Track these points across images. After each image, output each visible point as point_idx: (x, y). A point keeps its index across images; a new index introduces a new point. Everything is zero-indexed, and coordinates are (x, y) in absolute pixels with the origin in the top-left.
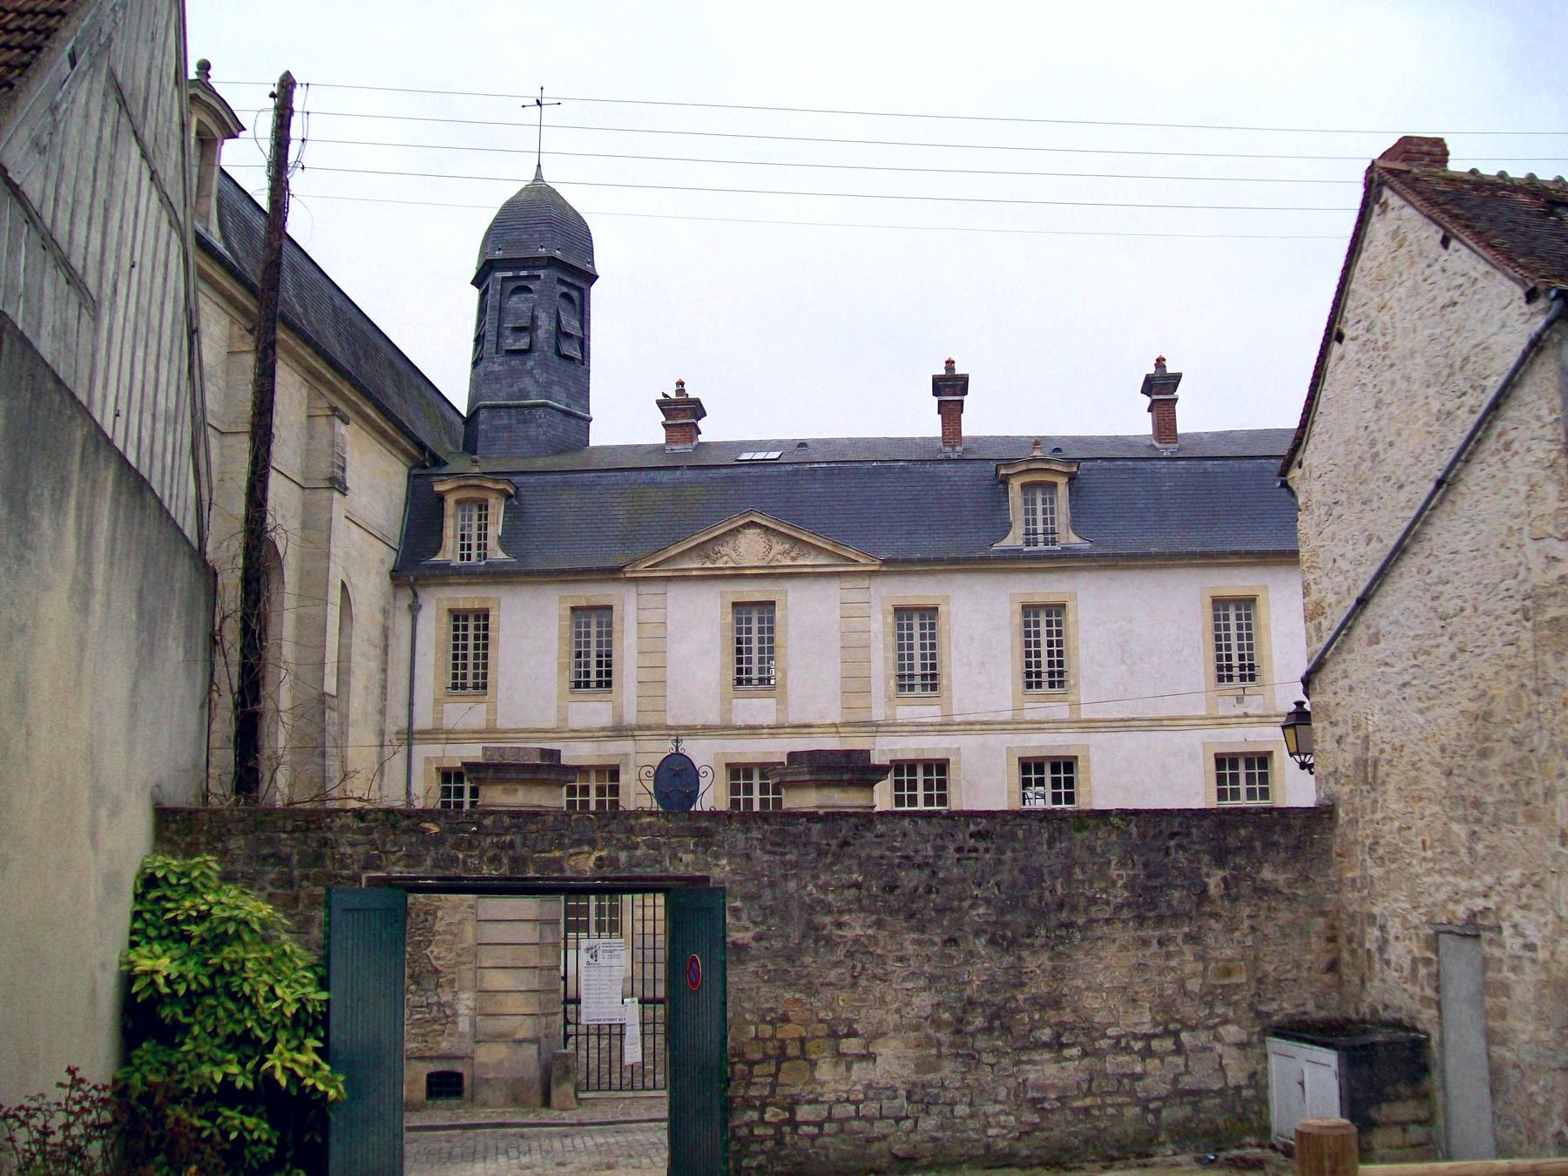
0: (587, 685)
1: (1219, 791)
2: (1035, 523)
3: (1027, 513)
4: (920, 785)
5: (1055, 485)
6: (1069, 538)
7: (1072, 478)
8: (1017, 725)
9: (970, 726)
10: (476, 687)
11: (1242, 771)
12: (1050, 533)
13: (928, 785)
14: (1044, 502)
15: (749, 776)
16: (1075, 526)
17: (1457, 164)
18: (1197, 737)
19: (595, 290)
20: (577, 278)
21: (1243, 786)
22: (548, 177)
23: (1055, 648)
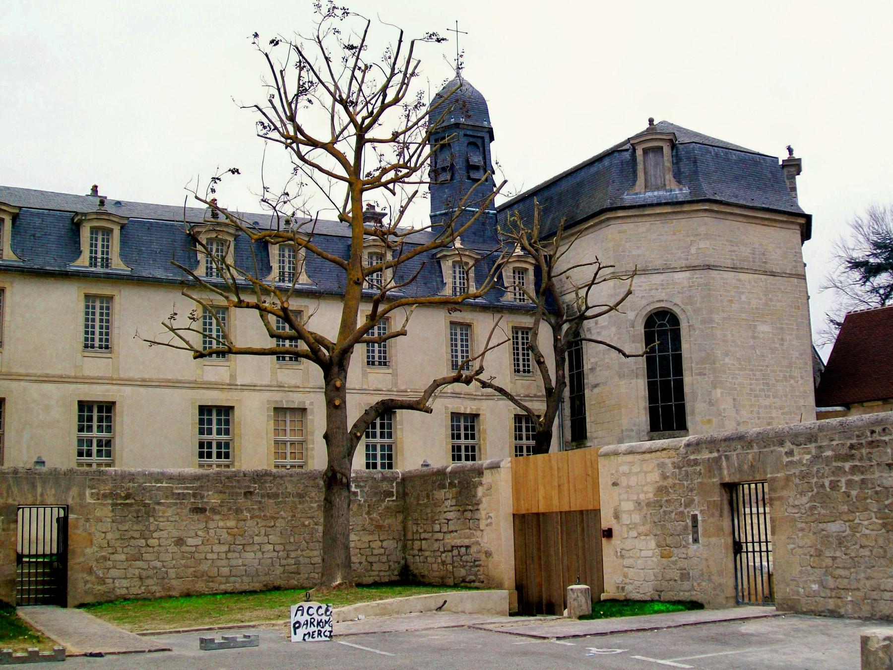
0: (373, 363)
1: (200, 429)
2: (96, 252)
3: (91, 245)
4: (214, 422)
5: (112, 230)
6: (118, 265)
7: (123, 227)
8: (268, 388)
9: (245, 387)
10: (101, 347)
11: (214, 418)
12: (106, 262)
13: (219, 422)
14: (103, 240)
15: (90, 410)
16: (123, 256)
17: (797, 177)
18: (267, 395)
19: (494, 148)
20: (482, 137)
21: (214, 427)
22: (465, 74)
23: (104, 330)
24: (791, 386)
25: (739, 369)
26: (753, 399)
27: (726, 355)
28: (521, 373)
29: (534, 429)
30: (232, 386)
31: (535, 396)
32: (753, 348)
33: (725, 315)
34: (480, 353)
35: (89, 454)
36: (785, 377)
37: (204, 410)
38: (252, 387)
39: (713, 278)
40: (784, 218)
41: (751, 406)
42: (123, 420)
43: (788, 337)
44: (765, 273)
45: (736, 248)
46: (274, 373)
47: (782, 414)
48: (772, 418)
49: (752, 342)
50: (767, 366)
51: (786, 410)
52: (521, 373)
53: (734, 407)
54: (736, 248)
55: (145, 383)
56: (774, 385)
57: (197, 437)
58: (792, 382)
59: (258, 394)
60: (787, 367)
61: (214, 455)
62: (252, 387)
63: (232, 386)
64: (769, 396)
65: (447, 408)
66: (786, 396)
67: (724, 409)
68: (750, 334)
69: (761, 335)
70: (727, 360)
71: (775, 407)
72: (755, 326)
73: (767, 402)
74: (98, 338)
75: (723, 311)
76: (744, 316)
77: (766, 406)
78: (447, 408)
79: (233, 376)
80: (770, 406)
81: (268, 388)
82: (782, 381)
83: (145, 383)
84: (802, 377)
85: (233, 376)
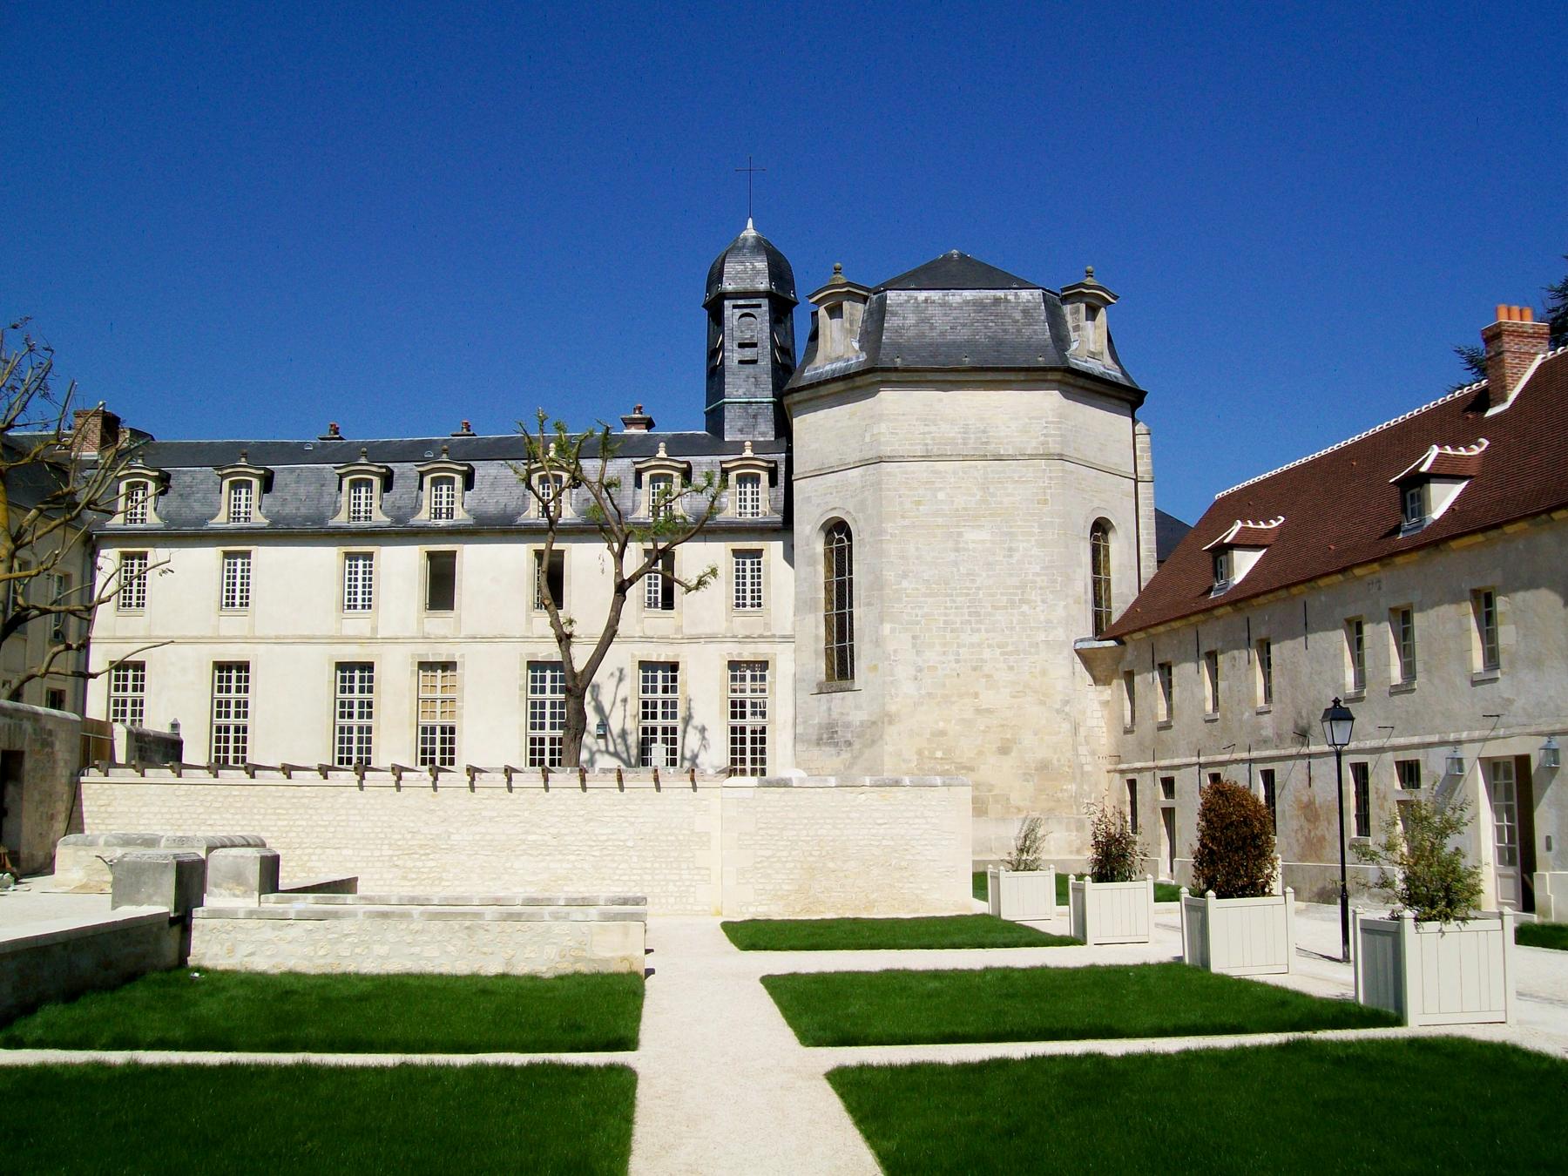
8: (411, 640)
24: (1023, 614)
25: (925, 595)
26: (948, 635)
27: (905, 575)
28: (748, 608)
29: (562, 679)
30: (372, 640)
31: (761, 636)
32: (956, 564)
33: (907, 522)
34: (632, 592)
35: (351, 715)
36: (1012, 602)
37: (221, 666)
38: (394, 640)
39: (889, 474)
40: (1021, 376)
41: (945, 645)
42: (258, 677)
43: (1021, 546)
44: (984, 458)
45: (933, 428)
46: (420, 622)
47: (1003, 654)
48: (982, 660)
49: (952, 556)
50: (979, 589)
51: (1010, 648)
52: (748, 608)
53: (914, 646)
54: (933, 428)
55: (279, 640)
56: (990, 614)
57: (250, 696)
58: (1025, 608)
59: (401, 647)
60: (1017, 588)
61: (659, 715)
62: (394, 640)
63: (372, 640)
64: (979, 630)
65: (633, 656)
66: (1012, 629)
67: (895, 651)
68: (950, 544)
69: (971, 546)
70: (905, 584)
71: (989, 646)
72: (960, 534)
73: (976, 638)
74: (235, 596)
75: (903, 517)
76: (940, 520)
77: (972, 645)
78: (633, 656)
79: (374, 629)
80: (980, 645)
81: (411, 640)
82: (1005, 608)
83: (279, 640)
84: (1043, 601)
85: (374, 629)
